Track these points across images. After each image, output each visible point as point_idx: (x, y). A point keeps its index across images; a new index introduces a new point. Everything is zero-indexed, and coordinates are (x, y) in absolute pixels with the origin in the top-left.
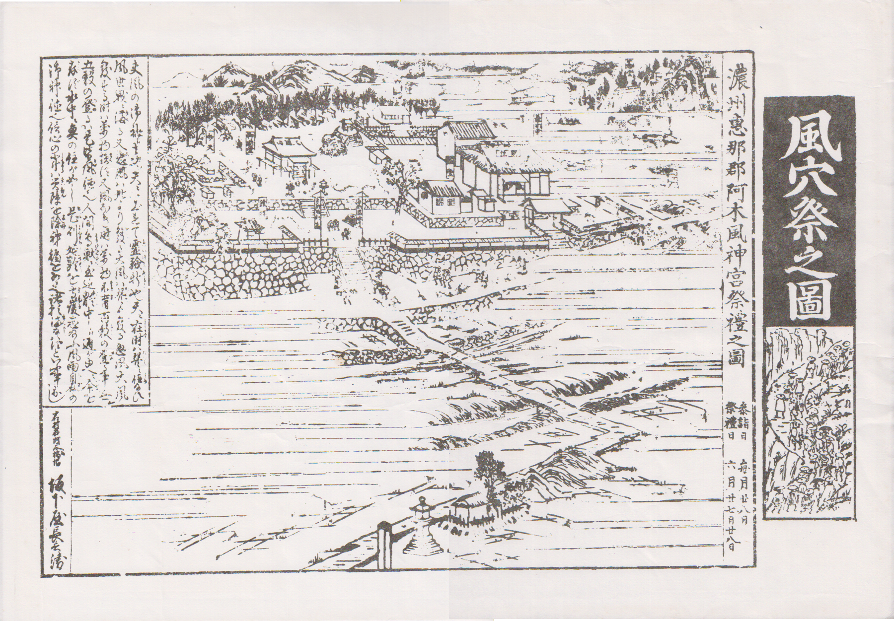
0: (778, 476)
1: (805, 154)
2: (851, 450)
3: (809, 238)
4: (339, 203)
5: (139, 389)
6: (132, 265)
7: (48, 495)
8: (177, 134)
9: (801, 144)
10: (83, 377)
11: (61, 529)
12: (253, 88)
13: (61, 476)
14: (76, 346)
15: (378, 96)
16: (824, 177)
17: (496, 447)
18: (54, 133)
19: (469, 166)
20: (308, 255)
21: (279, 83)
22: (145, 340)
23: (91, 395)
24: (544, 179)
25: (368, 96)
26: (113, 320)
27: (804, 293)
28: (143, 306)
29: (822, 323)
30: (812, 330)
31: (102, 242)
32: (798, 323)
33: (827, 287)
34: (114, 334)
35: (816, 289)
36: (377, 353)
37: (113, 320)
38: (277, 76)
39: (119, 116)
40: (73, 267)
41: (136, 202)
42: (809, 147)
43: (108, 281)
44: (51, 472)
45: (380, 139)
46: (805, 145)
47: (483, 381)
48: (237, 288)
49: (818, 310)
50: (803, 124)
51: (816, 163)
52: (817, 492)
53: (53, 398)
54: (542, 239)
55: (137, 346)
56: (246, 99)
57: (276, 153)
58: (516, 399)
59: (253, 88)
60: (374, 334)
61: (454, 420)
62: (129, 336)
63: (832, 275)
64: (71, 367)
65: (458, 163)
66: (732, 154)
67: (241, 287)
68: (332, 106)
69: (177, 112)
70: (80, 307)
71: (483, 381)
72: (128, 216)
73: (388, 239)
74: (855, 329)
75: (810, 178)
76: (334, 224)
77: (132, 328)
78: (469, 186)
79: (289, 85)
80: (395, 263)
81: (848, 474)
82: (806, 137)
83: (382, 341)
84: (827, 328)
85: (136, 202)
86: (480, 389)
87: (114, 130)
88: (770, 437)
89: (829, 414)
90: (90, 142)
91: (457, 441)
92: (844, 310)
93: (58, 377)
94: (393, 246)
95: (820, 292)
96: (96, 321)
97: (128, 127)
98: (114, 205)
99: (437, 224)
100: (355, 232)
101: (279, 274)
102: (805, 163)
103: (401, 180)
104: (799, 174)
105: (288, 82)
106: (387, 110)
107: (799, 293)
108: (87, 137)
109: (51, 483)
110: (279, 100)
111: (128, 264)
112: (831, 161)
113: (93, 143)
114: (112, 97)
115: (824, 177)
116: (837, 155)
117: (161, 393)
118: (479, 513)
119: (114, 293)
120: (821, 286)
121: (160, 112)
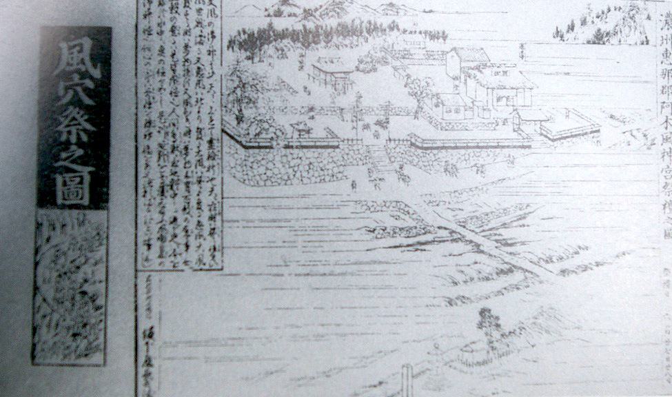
0: (44, 330)
1: (72, 73)
2: (103, 310)
3: (73, 139)
4: (370, 110)
5: (214, 257)
6: (209, 157)
7: (141, 342)
8: (244, 54)
9: (68, 64)
10: (169, 247)
11: (151, 369)
12: (305, 18)
13: (152, 328)
14: (164, 223)
15: (401, 28)
16: (86, 90)
17: (495, 305)
18: (147, 52)
19: (471, 82)
20: (347, 151)
21: (324, 15)
22: (218, 218)
23: (176, 261)
24: (528, 93)
25: (393, 27)
26: (194, 203)
27: (68, 183)
28: (217, 190)
29: (84, 208)
30: (75, 212)
31: (186, 139)
32: (63, 207)
33: (87, 179)
34: (194, 212)
35: (78, 180)
36: (401, 229)
37: (194, 203)
38: (322, 9)
39: (198, 39)
40: (162, 158)
41: (211, 108)
42: (75, 67)
43: (190, 170)
44: (144, 325)
45: (402, 60)
46: (72, 65)
47: (482, 252)
48: (292, 177)
49: (80, 197)
50: (71, 48)
51: (81, 79)
52: (74, 345)
53: (146, 264)
54: (526, 140)
55: (212, 222)
56: (299, 27)
57: (322, 70)
58: (507, 267)
59: (305, 18)
60: (398, 214)
61: (462, 283)
62: (206, 214)
63: (91, 169)
64: (162, 239)
65: (463, 80)
66: (664, 78)
67: (294, 175)
68: (365, 33)
69: (243, 37)
70: (167, 191)
71: (482, 252)
72: (206, 119)
73: (409, 138)
74: (108, 213)
75: (76, 92)
76: (366, 127)
77: (208, 208)
78: (472, 98)
79: (332, 16)
80: (415, 158)
81: (101, 330)
82: (72, 58)
83: (404, 220)
84: (87, 212)
85: (211, 108)
86: (479, 257)
87: (194, 49)
88: (39, 299)
89: (86, 281)
90: (175, 60)
91: (463, 298)
92: (99, 198)
93: (149, 246)
94: (412, 144)
95: (81, 183)
96: (180, 201)
97: (204, 49)
98: (195, 109)
99: (447, 128)
100: (384, 134)
101: (325, 165)
102: (71, 79)
103: (419, 93)
104: (67, 89)
105: (330, 14)
106: (408, 37)
107: (65, 184)
108: (173, 55)
109: (144, 332)
110: (324, 28)
111: (205, 157)
112: (92, 78)
113: (178, 61)
114: (193, 24)
115: (86, 90)
116: (97, 73)
117: (231, 261)
118: (480, 357)
119: (195, 180)
120: (82, 177)
121: (231, 37)
